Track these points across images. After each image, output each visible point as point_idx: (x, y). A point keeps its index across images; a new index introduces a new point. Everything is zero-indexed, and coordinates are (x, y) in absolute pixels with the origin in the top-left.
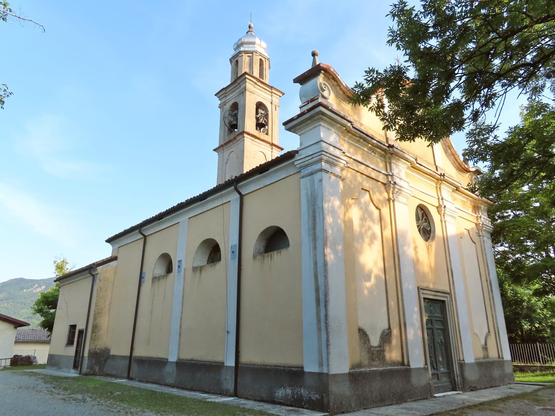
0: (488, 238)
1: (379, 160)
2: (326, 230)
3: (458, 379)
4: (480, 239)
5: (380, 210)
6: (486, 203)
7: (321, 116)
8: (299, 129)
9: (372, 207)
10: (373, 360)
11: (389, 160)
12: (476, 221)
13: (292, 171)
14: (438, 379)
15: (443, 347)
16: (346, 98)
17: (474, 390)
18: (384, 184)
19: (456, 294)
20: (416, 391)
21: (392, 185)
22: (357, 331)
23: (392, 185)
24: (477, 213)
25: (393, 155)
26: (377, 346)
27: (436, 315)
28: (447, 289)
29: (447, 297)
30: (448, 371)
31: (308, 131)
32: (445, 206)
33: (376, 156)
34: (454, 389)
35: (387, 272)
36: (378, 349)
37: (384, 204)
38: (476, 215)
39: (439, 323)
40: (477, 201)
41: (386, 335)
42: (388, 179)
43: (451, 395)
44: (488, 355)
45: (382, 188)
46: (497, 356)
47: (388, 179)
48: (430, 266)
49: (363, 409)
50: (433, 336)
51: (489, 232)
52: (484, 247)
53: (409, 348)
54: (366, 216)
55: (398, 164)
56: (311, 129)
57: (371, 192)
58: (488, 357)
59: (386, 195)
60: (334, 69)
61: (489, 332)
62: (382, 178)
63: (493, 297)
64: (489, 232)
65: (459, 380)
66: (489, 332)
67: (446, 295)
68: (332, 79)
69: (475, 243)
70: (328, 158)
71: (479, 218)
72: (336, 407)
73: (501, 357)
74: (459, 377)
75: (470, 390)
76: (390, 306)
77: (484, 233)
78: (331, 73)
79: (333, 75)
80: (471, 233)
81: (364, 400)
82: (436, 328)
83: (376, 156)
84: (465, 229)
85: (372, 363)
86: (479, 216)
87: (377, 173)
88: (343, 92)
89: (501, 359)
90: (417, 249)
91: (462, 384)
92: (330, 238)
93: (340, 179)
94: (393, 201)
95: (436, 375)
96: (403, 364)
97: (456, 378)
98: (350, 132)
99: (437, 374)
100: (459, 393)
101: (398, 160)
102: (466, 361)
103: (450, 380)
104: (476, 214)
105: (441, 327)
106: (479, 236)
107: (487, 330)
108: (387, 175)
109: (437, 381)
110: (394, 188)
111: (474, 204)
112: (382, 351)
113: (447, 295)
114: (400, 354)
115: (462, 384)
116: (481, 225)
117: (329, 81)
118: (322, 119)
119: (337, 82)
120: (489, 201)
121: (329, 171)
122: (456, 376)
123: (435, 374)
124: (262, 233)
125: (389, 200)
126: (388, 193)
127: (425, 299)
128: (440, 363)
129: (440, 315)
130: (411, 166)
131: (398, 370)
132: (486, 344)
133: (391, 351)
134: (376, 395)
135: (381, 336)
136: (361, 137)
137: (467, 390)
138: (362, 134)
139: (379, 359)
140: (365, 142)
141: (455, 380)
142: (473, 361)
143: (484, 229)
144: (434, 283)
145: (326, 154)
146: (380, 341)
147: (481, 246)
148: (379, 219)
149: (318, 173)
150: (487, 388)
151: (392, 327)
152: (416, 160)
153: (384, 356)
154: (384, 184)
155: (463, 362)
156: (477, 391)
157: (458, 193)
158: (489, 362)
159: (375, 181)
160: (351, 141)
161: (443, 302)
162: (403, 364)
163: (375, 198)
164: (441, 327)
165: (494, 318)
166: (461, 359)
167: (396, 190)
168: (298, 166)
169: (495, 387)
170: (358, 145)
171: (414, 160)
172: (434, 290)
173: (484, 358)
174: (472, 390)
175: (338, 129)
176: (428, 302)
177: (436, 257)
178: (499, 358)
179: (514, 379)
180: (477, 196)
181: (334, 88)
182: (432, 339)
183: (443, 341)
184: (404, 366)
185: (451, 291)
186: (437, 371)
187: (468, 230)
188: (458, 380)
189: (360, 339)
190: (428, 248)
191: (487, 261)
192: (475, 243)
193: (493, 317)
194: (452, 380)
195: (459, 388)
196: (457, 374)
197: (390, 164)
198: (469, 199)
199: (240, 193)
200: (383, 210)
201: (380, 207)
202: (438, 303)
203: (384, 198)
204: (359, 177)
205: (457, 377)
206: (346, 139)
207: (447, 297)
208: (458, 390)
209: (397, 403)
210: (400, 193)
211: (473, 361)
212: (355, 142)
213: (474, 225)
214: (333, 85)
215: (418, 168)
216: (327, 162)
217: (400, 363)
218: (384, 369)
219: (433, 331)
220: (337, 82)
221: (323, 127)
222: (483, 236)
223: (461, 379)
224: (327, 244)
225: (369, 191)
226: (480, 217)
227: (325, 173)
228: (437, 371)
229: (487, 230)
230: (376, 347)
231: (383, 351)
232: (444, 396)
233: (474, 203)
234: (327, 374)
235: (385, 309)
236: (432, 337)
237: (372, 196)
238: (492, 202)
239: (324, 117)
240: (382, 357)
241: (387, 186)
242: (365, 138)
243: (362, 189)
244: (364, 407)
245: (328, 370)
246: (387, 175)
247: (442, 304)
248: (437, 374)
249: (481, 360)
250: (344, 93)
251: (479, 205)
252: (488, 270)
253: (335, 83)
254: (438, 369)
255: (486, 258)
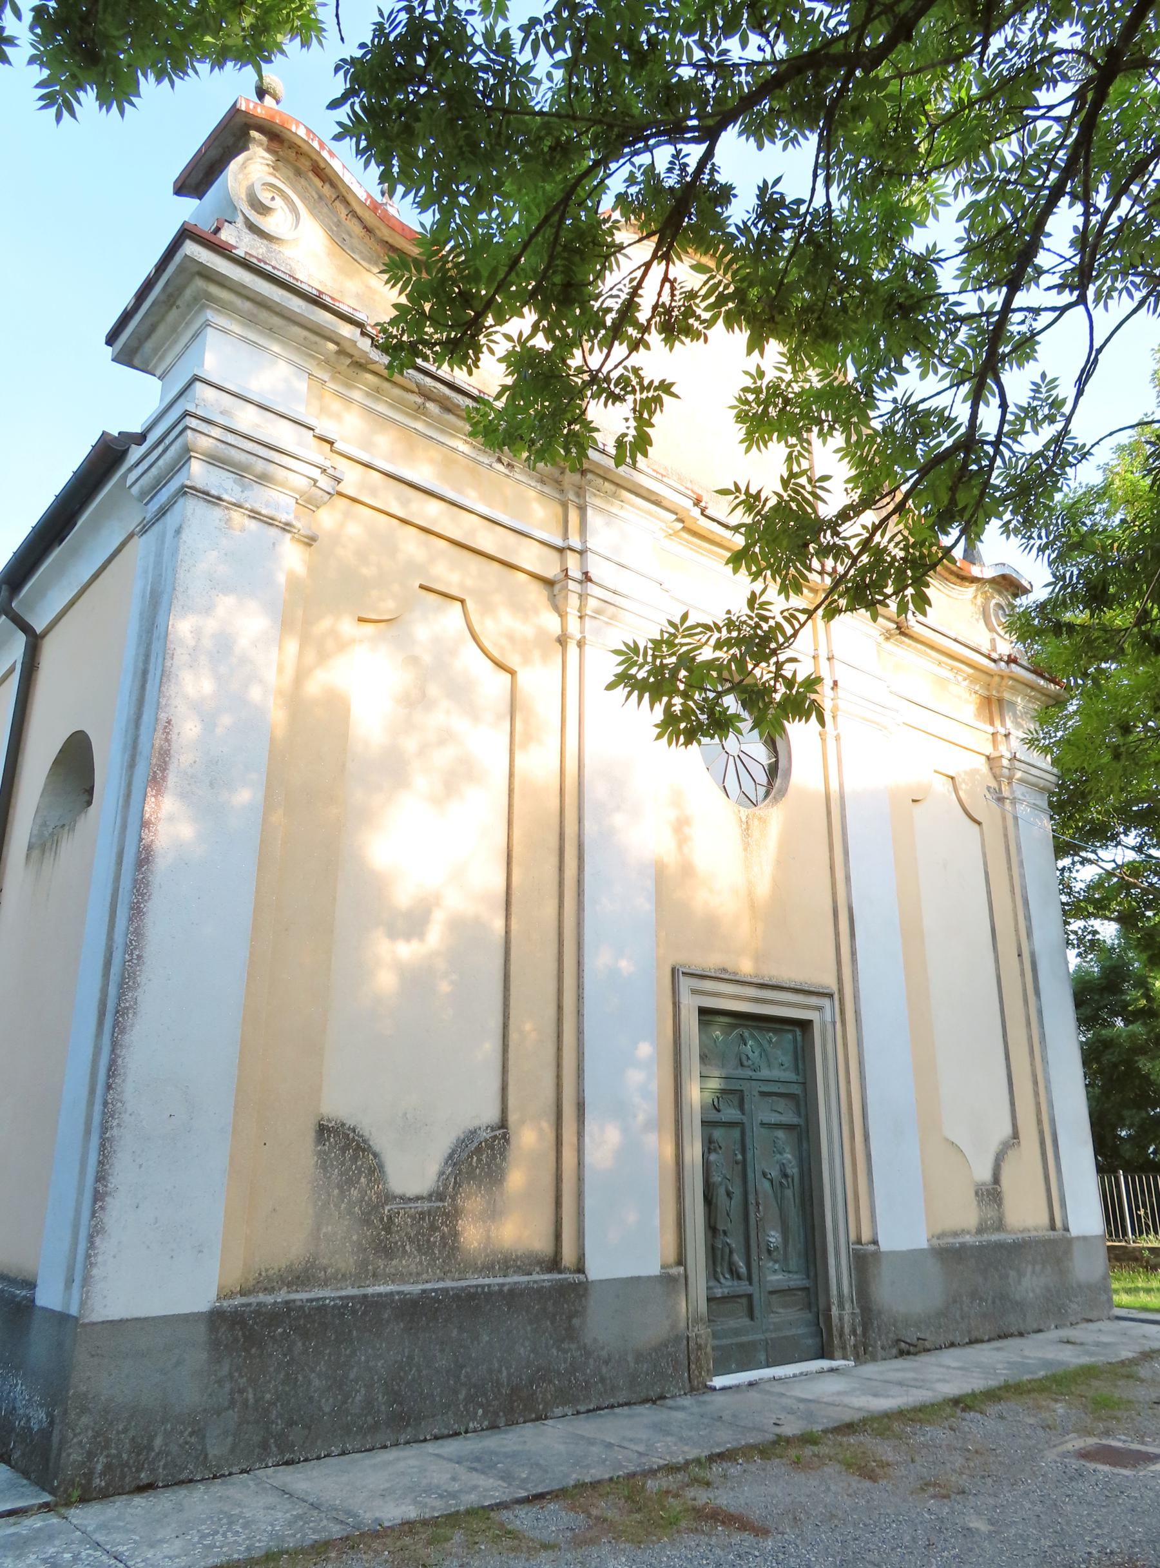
0: (1035, 806)
1: (532, 494)
2: (169, 722)
3: (844, 1315)
4: (1003, 811)
5: (512, 673)
6: (1033, 688)
7: (199, 283)
8: (155, 351)
9: (471, 660)
10: (387, 1251)
11: (578, 495)
12: (988, 749)
13: (132, 517)
14: (751, 1316)
15: (789, 1193)
16: (381, 251)
17: (915, 1354)
18: (549, 583)
19: (512, 979)
20: (604, 1370)
21: (572, 585)
22: (311, 1135)
23: (572, 585)
24: (997, 723)
25: (589, 476)
26: (425, 1194)
27: (765, 1073)
28: (828, 981)
29: (820, 1009)
30: (805, 1283)
31: (179, 357)
32: (835, 683)
33: (518, 476)
34: (824, 1353)
35: (514, 909)
36: (426, 1206)
37: (536, 654)
38: (991, 730)
39: (781, 1104)
40: (997, 679)
41: (478, 1150)
42: (563, 561)
43: (795, 1376)
44: (1001, 1219)
45: (536, 594)
46: (1044, 1220)
47: (563, 561)
48: (750, 894)
49: (241, 1473)
50: (744, 1151)
51: (1043, 789)
52: (1017, 837)
53: (589, 1202)
54: (433, 690)
55: (614, 510)
56: (187, 347)
57: (470, 604)
58: (1000, 1226)
59: (551, 622)
60: (309, 131)
61: (1016, 1135)
62: (531, 557)
63: (1040, 1012)
64: (1043, 789)
65: (846, 1318)
66: (1016, 1135)
67: (813, 1001)
68: (311, 175)
69: (979, 823)
70: (219, 444)
71: (999, 738)
72: (99, 1467)
73: (1059, 1224)
74: (847, 1306)
75: (894, 1351)
76: (514, 1036)
77: (1019, 791)
78: (299, 143)
79: (315, 157)
80: (964, 786)
81: (291, 1423)
82: (762, 1124)
83: (518, 476)
84: (936, 771)
85: (381, 1263)
86: (1003, 731)
87: (512, 538)
88: (365, 227)
89: (1060, 1233)
90: (686, 829)
91: (859, 1332)
92: (184, 759)
93: (289, 536)
94: (580, 644)
95: (744, 1301)
96: (554, 1263)
97: (835, 1311)
98: (371, 367)
99: (750, 1297)
100: (832, 1370)
101: (614, 495)
102: (885, 1245)
103: (809, 1316)
104: (992, 723)
105: (789, 1118)
106: (1001, 800)
107: (1007, 1130)
108: (561, 550)
109: (746, 1321)
110: (582, 597)
111: (988, 690)
112: (447, 1215)
113: (826, 1002)
114: (547, 1228)
115: (859, 1332)
116: (1005, 762)
117: (302, 181)
118: (210, 298)
119: (333, 185)
120: (1042, 682)
121: (225, 497)
122: (834, 1300)
123: (739, 1296)
124: (57, 762)
125: (562, 641)
126: (562, 615)
127: (703, 1011)
128: (769, 1252)
129: (790, 1076)
130: (680, 525)
131: (511, 1291)
132: (996, 1179)
133: (493, 1213)
134: (369, 1402)
135: (451, 1156)
136: (427, 396)
137: (881, 1353)
138: (428, 381)
139: (425, 1248)
140: (451, 418)
141: (829, 1318)
142: (920, 1240)
143: (1019, 775)
144: (757, 958)
145: (203, 427)
146: (442, 1173)
147: (1006, 836)
148: (504, 707)
149: (176, 506)
150: (982, 1341)
151: (513, 1118)
152: (697, 502)
153: (455, 1235)
154: (549, 583)
155: (872, 1248)
156: (924, 1358)
157: (909, 646)
158: (1000, 1246)
159: (496, 565)
160: (381, 408)
161: (805, 1026)
162: (554, 1263)
163: (488, 628)
164: (789, 1117)
165: (1040, 1083)
166: (866, 1237)
167: (592, 603)
168: (135, 490)
169: (1021, 1335)
170: (419, 426)
171: (688, 504)
172: (755, 980)
173: (980, 1231)
174: (902, 1353)
175: (308, 350)
176: (734, 1027)
177: (786, 859)
178: (1053, 1227)
179: (1110, 1300)
180: (994, 661)
181: (325, 210)
182: (737, 1163)
183: (793, 1171)
184: (560, 1272)
185: (841, 990)
186: (751, 1284)
187: (952, 778)
188: (841, 1318)
189: (324, 1164)
190: (748, 829)
191: (1024, 888)
192: (979, 823)
193: (1035, 1083)
194: (820, 1316)
195: (844, 1348)
196: (840, 1295)
197: (582, 509)
198: (959, 670)
199: (26, 628)
200: (524, 677)
201: (513, 661)
202: (782, 1030)
203: (541, 633)
204: (411, 544)
205: (841, 1306)
206: (357, 395)
207: (820, 1009)
208: (838, 1353)
209: (493, 1427)
210: (613, 617)
211: (924, 1245)
212: (408, 414)
213: (981, 765)
214: (321, 197)
215: (718, 540)
216: (215, 460)
217: (539, 1263)
218: (434, 1290)
219: (743, 1134)
220: (333, 185)
221: (225, 331)
222: (1014, 801)
223: (857, 1311)
224: (164, 779)
225: (462, 601)
226: (1007, 736)
227: (202, 504)
228: (751, 1284)
229: (1034, 780)
230: (418, 1198)
231: (452, 1215)
232: (751, 1384)
233: (988, 686)
234: (76, 1319)
235: (490, 1047)
236: (740, 1157)
237: (474, 618)
238: (1056, 683)
239: (214, 290)
240: (443, 1237)
241: (557, 587)
242: (448, 398)
243: (422, 587)
244: (287, 1456)
245: (83, 1304)
246: (561, 550)
247: (798, 1033)
248: (750, 1297)
249: (968, 1239)
250: (368, 229)
251: (1007, 696)
252: (1028, 918)
253: (327, 190)
254: (755, 1277)
255: (1023, 876)
